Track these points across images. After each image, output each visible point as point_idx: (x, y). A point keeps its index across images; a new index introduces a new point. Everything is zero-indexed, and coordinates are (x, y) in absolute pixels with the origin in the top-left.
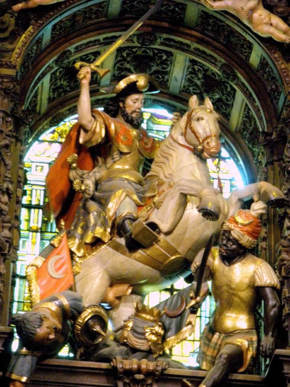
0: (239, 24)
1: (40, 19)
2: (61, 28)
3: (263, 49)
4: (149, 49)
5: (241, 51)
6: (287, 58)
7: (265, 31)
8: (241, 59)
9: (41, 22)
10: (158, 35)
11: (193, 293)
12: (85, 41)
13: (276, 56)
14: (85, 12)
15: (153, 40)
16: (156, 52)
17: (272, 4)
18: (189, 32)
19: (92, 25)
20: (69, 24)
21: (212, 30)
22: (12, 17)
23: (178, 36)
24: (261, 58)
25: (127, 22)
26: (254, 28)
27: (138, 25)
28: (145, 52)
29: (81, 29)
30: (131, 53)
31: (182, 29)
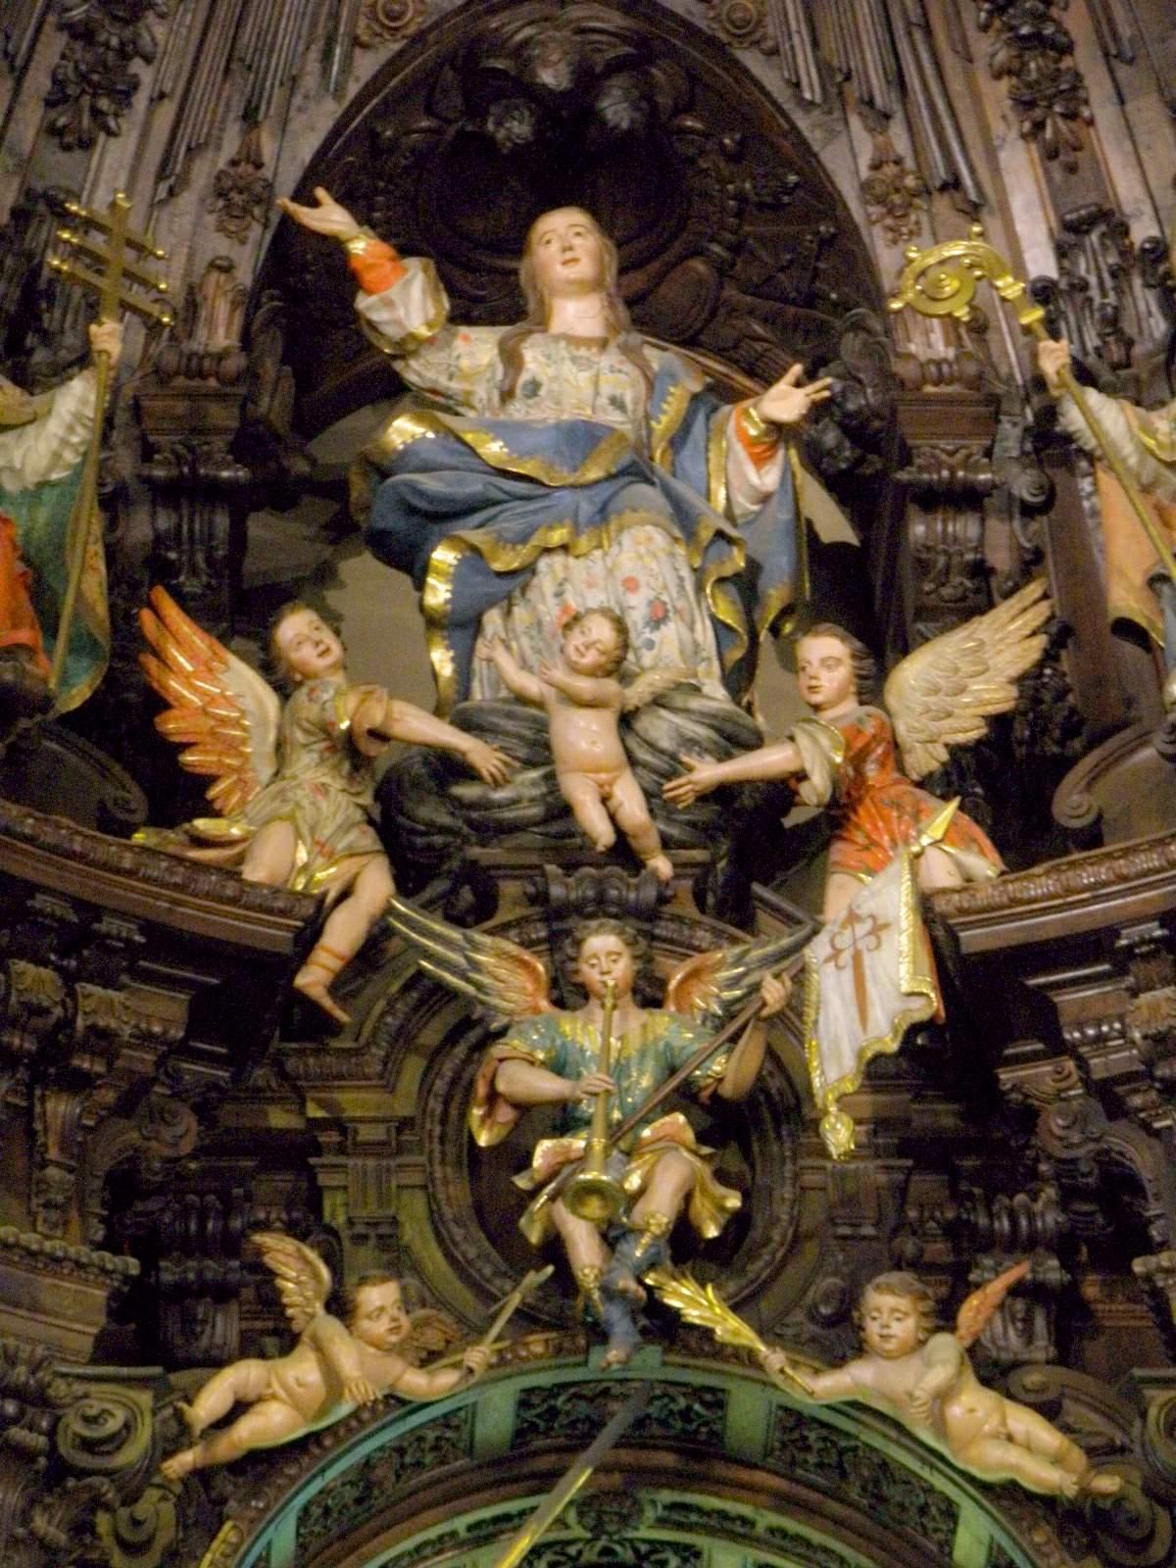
0: (904, 1440)
1: (256, 1494)
2: (327, 1511)
3: (995, 1519)
4: (620, 1543)
5: (923, 1526)
6: (1074, 1544)
7: (994, 1460)
8: (925, 1554)
9: (261, 1505)
10: (643, 1495)
11: (563, 68)
12: (409, 1544)
13: (1038, 1538)
14: (401, 1451)
15: (630, 1515)
16: (644, 1548)
17: (1004, 1356)
18: (744, 1475)
19: (430, 1485)
20: (350, 1494)
21: (820, 1465)
22: (163, 1498)
23: (710, 1494)
24: (991, 1548)
25: (543, 1463)
26: (955, 1453)
27: (577, 1478)
28: (606, 1551)
29: (394, 1504)
30: (563, 1559)
31: (720, 1469)
